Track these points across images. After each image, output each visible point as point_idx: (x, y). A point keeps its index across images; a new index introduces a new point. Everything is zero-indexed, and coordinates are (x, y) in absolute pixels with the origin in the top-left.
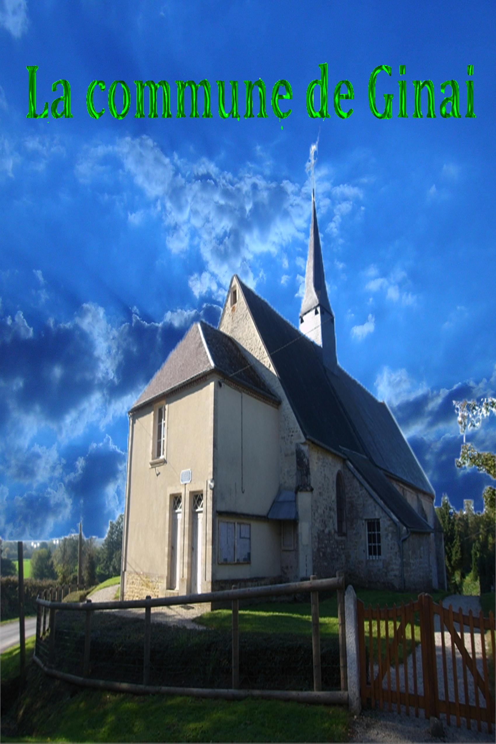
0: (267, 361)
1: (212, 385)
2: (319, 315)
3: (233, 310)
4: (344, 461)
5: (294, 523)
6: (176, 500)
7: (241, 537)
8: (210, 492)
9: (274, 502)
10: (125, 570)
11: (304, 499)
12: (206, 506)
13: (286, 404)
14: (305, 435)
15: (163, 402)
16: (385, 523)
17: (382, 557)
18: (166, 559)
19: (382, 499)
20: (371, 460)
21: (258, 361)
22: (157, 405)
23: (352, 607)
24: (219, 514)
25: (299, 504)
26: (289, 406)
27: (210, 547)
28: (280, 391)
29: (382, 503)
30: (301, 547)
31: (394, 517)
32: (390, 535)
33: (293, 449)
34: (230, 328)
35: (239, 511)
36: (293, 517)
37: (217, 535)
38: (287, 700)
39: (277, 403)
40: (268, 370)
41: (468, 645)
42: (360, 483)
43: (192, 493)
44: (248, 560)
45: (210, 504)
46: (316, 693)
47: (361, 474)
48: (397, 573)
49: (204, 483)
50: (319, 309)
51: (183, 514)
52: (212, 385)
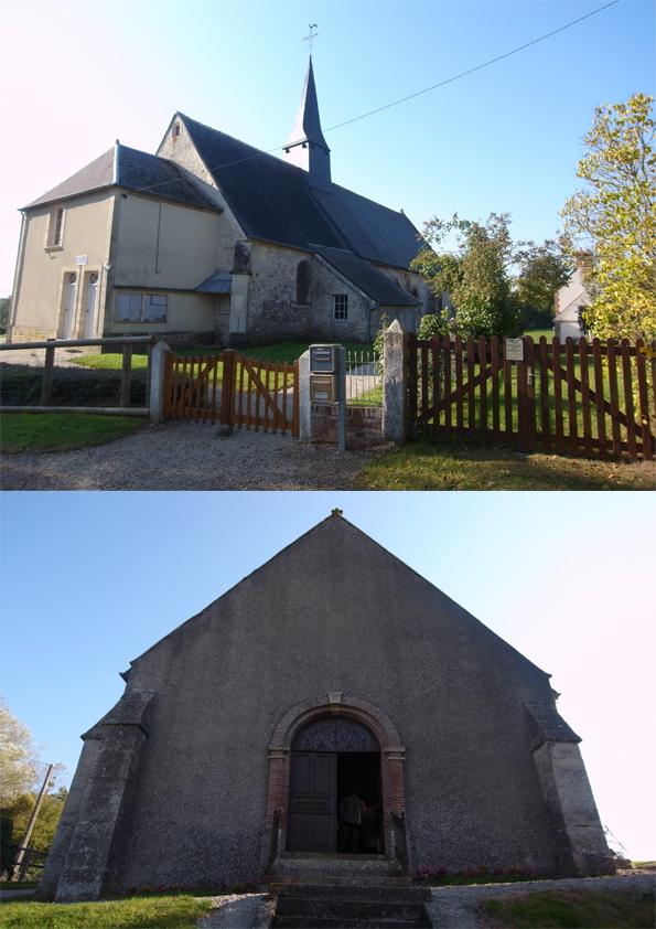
0: (209, 179)
1: (113, 198)
2: (307, 150)
3: (175, 140)
4: (312, 254)
5: (226, 296)
6: (71, 277)
7: (151, 304)
8: (105, 273)
9: (207, 281)
10: (14, 324)
11: (240, 281)
12: (101, 286)
13: (228, 213)
14: (247, 234)
15: (61, 206)
16: (352, 298)
17: (349, 319)
18: (58, 317)
19: (350, 280)
20: (357, 254)
21: (200, 180)
22: (57, 207)
23: (159, 356)
24: (113, 288)
25: (233, 282)
26: (232, 214)
27: (103, 311)
28: (223, 203)
29: (351, 284)
30: (232, 312)
31: (363, 294)
32: (358, 307)
33: (234, 244)
34: (170, 153)
35: (149, 285)
36: (225, 291)
37: (114, 303)
38: (102, 414)
39: (219, 211)
40: (210, 187)
41: (263, 380)
42: (330, 271)
43: (66, 274)
44: (164, 319)
45: (105, 280)
46: (41, 408)
47: (329, 263)
48: (363, 331)
49: (102, 264)
50: (307, 144)
51: (78, 285)
52: (113, 198)
